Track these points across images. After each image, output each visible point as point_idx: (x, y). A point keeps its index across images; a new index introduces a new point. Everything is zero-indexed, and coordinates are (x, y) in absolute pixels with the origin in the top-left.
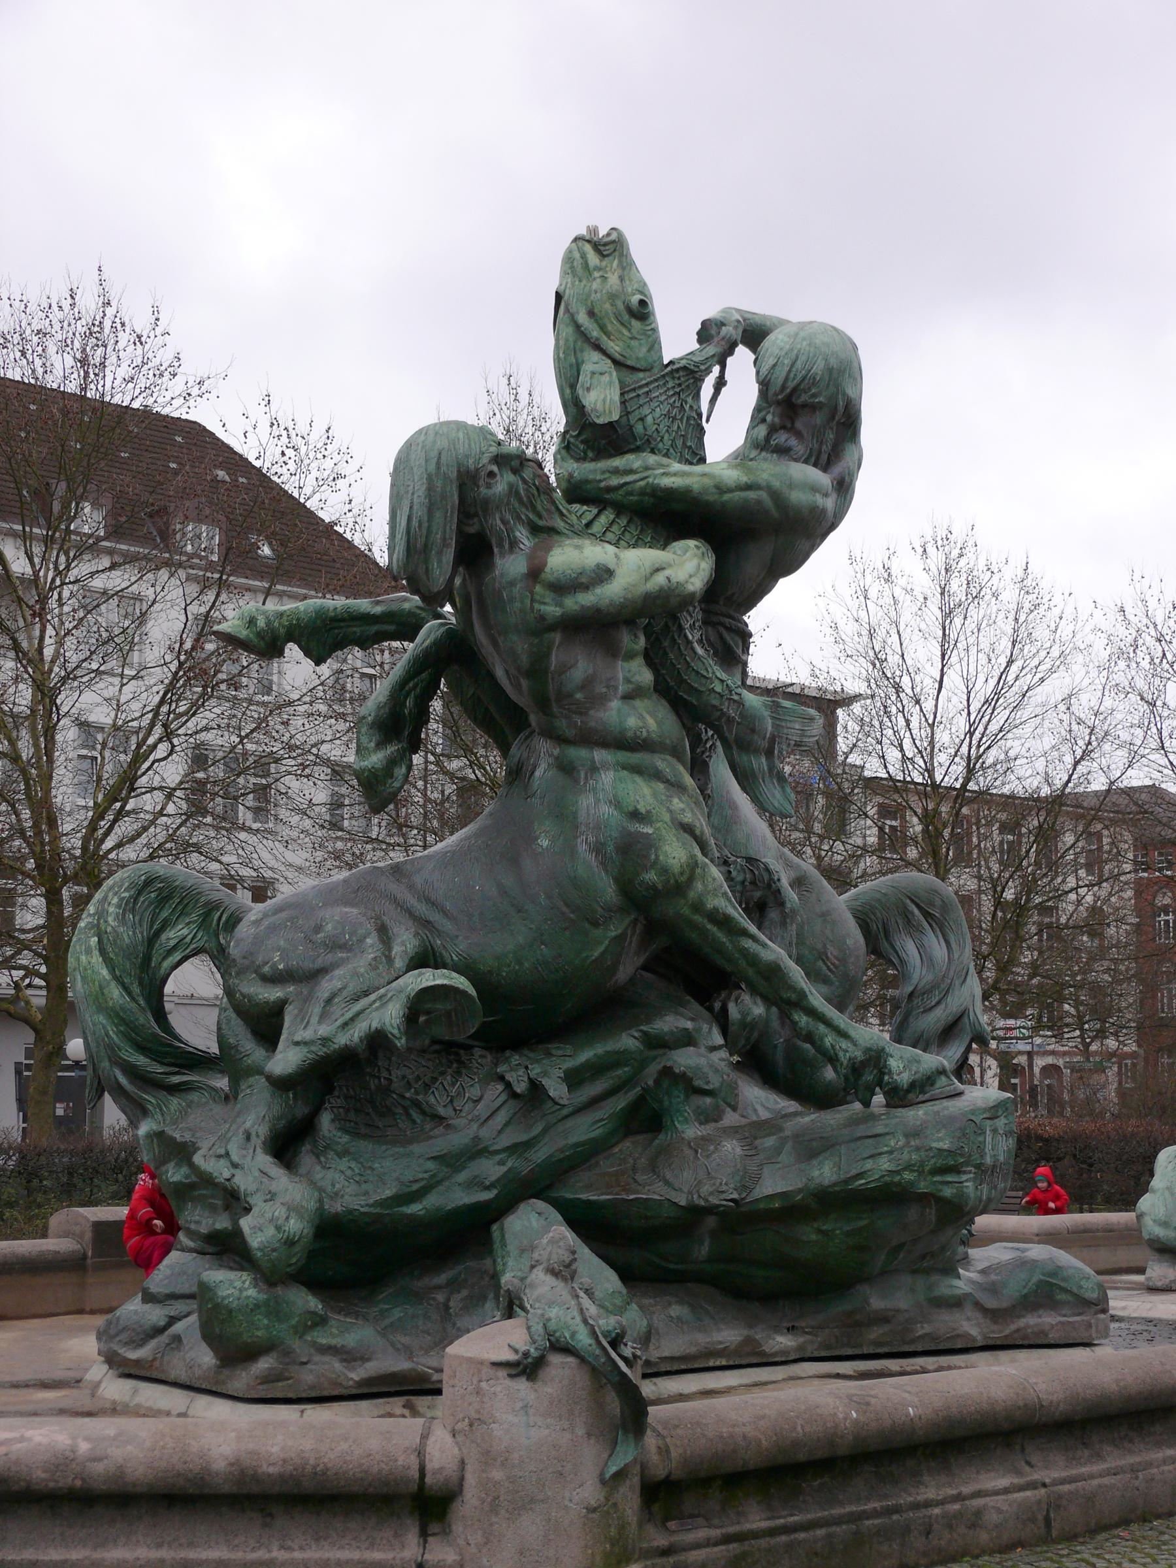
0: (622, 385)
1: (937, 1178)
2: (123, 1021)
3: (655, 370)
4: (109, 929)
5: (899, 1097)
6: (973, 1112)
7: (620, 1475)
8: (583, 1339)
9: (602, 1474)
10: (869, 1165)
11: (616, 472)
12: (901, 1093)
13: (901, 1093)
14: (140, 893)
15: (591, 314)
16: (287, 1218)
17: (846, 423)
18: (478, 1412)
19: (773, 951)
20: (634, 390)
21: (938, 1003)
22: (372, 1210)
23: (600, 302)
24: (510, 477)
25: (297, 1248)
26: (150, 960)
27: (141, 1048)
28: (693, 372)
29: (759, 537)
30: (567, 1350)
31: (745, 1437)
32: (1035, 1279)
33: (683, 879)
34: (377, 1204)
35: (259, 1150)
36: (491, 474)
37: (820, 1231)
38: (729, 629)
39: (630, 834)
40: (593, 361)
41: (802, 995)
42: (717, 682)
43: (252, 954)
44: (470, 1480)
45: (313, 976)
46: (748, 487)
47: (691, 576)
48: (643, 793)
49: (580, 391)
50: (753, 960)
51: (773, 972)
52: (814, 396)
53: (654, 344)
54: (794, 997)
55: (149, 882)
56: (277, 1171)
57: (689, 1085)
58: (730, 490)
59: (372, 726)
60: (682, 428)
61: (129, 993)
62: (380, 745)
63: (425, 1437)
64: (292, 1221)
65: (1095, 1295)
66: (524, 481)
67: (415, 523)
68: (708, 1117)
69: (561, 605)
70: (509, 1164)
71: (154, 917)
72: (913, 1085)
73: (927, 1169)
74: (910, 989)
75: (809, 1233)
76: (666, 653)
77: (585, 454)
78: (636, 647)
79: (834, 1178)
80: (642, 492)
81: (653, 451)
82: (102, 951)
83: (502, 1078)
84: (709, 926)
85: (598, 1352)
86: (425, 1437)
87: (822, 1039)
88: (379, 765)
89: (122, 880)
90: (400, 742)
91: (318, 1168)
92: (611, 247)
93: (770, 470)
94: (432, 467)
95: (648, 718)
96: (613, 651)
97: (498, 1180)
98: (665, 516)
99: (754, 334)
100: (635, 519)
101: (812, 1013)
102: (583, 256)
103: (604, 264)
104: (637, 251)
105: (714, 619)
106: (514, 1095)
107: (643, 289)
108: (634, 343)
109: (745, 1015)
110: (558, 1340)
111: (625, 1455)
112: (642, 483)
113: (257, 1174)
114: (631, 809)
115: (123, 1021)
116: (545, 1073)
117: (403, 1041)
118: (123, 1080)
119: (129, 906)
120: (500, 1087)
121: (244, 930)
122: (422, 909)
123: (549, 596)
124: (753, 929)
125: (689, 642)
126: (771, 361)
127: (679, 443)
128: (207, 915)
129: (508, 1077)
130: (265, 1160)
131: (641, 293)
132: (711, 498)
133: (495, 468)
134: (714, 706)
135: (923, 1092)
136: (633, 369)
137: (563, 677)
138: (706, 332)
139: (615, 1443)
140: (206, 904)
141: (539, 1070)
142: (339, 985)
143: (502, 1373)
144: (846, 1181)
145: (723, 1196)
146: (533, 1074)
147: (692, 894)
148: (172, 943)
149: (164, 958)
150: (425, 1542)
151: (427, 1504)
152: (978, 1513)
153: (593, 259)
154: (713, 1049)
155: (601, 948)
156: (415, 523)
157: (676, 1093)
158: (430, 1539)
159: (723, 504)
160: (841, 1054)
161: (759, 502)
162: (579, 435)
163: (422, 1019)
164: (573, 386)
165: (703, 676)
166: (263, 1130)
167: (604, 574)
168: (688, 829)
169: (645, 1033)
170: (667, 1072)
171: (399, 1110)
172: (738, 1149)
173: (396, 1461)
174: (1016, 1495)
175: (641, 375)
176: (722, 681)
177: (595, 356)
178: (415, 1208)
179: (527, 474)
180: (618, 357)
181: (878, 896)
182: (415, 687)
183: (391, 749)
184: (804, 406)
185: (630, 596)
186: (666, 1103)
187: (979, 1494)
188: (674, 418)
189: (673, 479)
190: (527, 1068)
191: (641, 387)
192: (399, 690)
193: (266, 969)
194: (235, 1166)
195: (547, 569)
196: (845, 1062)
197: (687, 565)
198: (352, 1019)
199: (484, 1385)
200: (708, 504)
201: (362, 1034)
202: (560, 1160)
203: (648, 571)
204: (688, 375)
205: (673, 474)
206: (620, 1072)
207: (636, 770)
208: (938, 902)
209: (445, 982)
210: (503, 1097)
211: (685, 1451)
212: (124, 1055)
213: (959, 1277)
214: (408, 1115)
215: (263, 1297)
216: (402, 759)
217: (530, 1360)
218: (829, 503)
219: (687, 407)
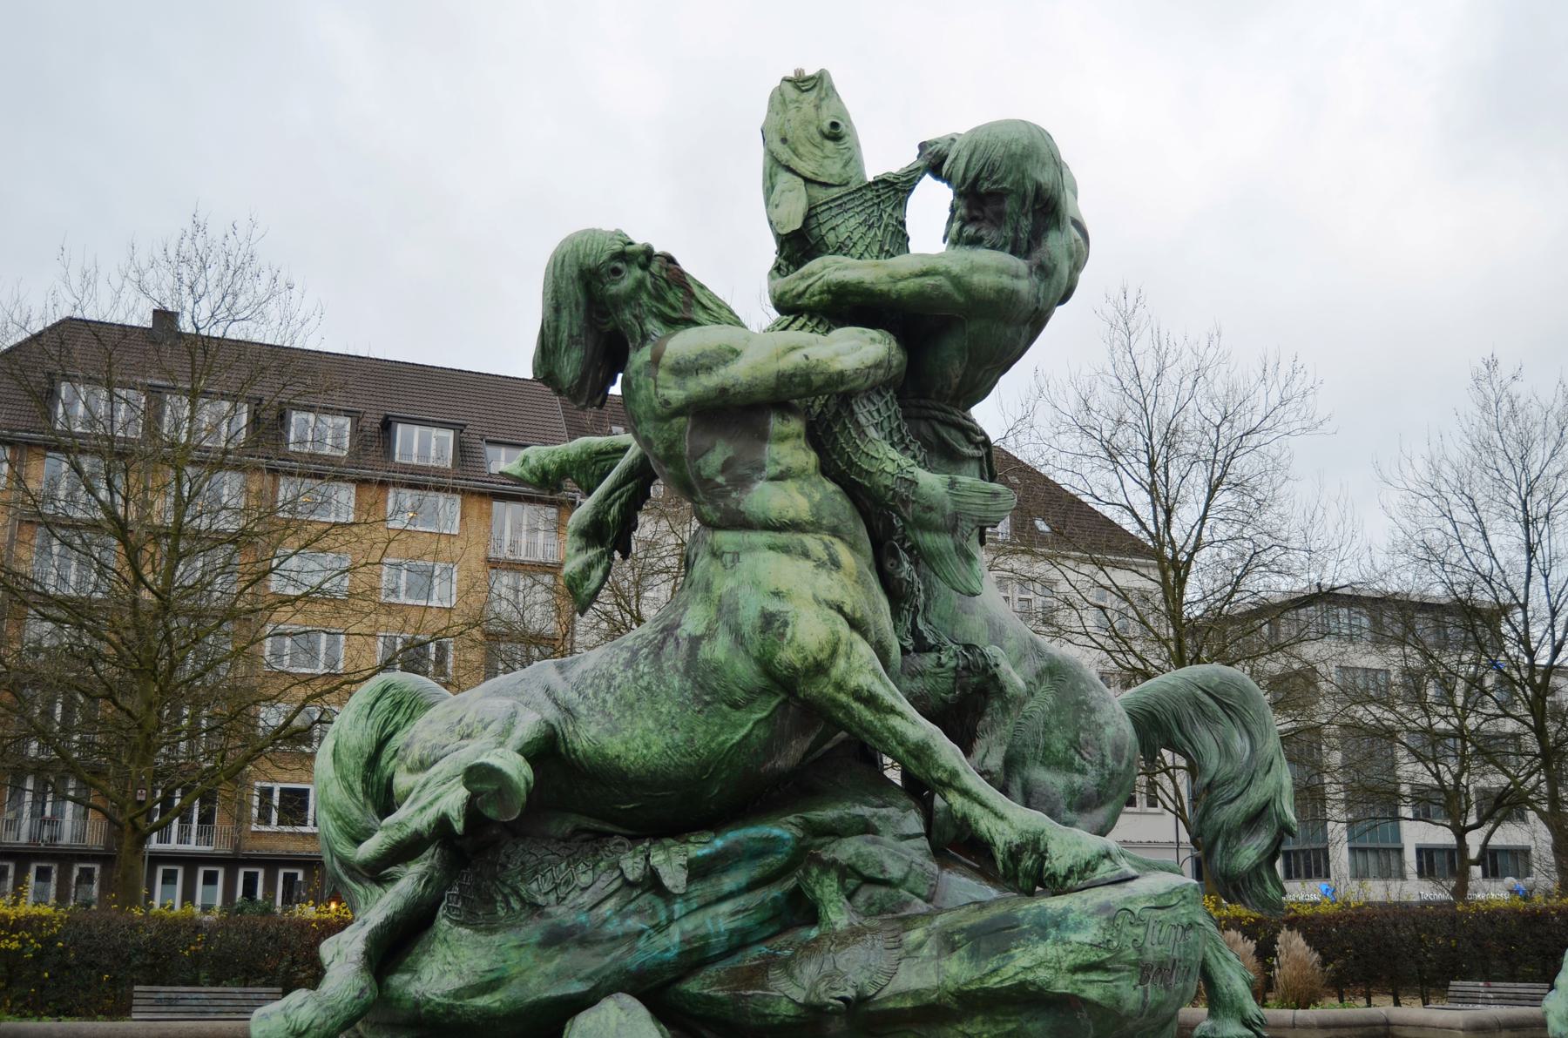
0: (809, 197)
1: (1080, 976)
2: (340, 816)
15: (784, 140)
21: (1241, 794)
22: (445, 1001)
24: (638, 273)
28: (893, 184)
33: (823, 656)
36: (616, 272)
40: (784, 178)
41: (954, 774)
42: (889, 462)
52: (995, 182)
53: (852, 159)
54: (945, 777)
55: (385, 691)
57: (855, 878)
58: (904, 278)
61: (350, 789)
66: (652, 275)
69: (682, 387)
73: (1065, 965)
74: (1206, 780)
76: (836, 439)
80: (821, 293)
92: (811, 83)
98: (845, 307)
101: (965, 793)
105: (925, 412)
108: (827, 162)
115: (340, 816)
123: (671, 380)
132: (884, 287)
133: (620, 265)
137: (701, 461)
145: (834, 994)
153: (791, 92)
155: (743, 732)
157: (827, 882)
159: (899, 294)
161: (937, 287)
169: (807, 821)
175: (836, 190)
177: (787, 176)
178: (482, 1001)
180: (809, 175)
182: (620, 497)
183: (592, 553)
184: (990, 194)
185: (758, 374)
186: (818, 892)
188: (871, 227)
195: (666, 354)
197: (856, 349)
200: (883, 295)
206: (770, 859)
207: (785, 549)
208: (1234, 692)
212: (339, 848)
214: (508, 903)
216: (599, 562)
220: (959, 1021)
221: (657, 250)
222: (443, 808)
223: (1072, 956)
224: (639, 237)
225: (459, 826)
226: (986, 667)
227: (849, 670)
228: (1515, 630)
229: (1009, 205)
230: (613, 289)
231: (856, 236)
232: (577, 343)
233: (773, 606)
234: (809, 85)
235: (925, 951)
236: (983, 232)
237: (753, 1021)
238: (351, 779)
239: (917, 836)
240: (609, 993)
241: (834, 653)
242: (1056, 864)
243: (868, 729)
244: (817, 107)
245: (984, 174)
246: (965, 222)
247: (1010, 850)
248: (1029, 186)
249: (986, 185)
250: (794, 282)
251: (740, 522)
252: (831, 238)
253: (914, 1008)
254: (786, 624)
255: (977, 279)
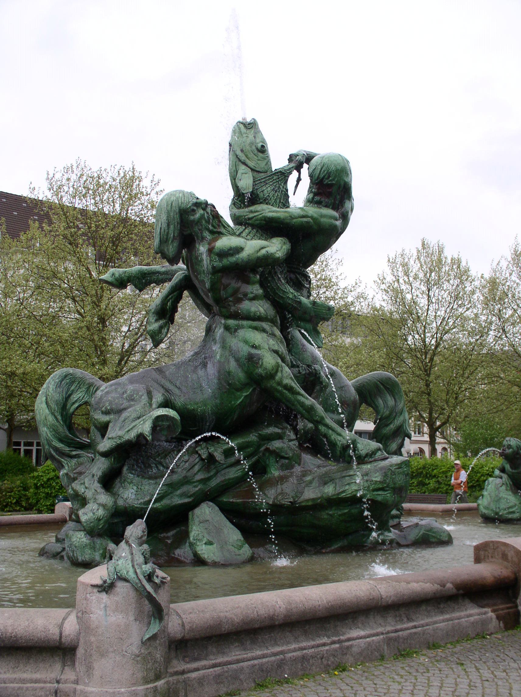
1: (375, 493)
3: (268, 172)
4: (50, 394)
5: (362, 460)
6: (391, 466)
7: (154, 637)
8: (131, 575)
9: (142, 639)
10: (347, 487)
11: (251, 212)
12: (362, 458)
13: (362, 458)
14: (62, 380)
15: (242, 151)
16: (98, 509)
17: (345, 191)
18: (85, 608)
19: (311, 400)
20: (259, 180)
23: (247, 148)
24: (202, 212)
25: (102, 522)
26: (66, 406)
27: (61, 441)
28: (284, 173)
29: (311, 239)
30: (126, 580)
31: (226, 617)
32: (421, 533)
34: (141, 504)
35: (96, 482)
37: (328, 514)
38: (299, 274)
39: (252, 354)
40: (242, 168)
41: (322, 418)
43: (99, 403)
44: (82, 641)
45: (119, 412)
46: (303, 217)
47: (277, 251)
48: (257, 337)
49: (237, 180)
50: (302, 405)
51: (310, 410)
52: (331, 181)
53: (268, 163)
55: (66, 376)
56: (100, 490)
57: (278, 455)
58: (296, 218)
59: (153, 313)
60: (279, 195)
61: (57, 419)
62: (156, 321)
63: (64, 619)
64: (100, 511)
65: (447, 539)
67: (163, 230)
68: (285, 467)
69: (221, 261)
70: (199, 487)
71: (68, 389)
72: (367, 455)
75: (324, 515)
77: (241, 206)
78: (255, 279)
79: (333, 493)
80: (261, 219)
81: (267, 204)
82: (47, 403)
83: (197, 452)
84: (284, 391)
85: (137, 581)
86: (64, 619)
87: (330, 436)
88: (156, 329)
89: (56, 375)
90: (165, 319)
91: (121, 488)
93: (313, 211)
94: (169, 208)
95: (261, 307)
96: (247, 281)
97: (194, 494)
98: (269, 228)
99: (309, 158)
100: (259, 230)
101: (327, 426)
102: (240, 129)
103: (248, 132)
104: (262, 127)
106: (202, 460)
107: (264, 141)
109: (305, 426)
110: (121, 575)
111: (155, 628)
112: (261, 216)
113: (93, 491)
114: (252, 344)
116: (216, 450)
117: (150, 437)
118: (54, 454)
119: (59, 385)
120: (197, 456)
121: (99, 393)
122: (168, 385)
124: (303, 392)
125: (279, 278)
126: (314, 168)
127: (278, 201)
128: (88, 388)
129: (199, 452)
130: (97, 486)
131: (263, 142)
132: (288, 221)
134: (289, 303)
135: (371, 457)
136: (259, 172)
138: (291, 158)
139: (149, 623)
140: (88, 384)
141: (213, 449)
142: (128, 415)
143: (95, 590)
144: (338, 494)
145: (286, 500)
146: (210, 451)
147: (277, 378)
148: (75, 399)
149: (72, 406)
150: (64, 669)
151: (61, 650)
152: (348, 648)
154: (291, 440)
156: (163, 230)
158: (66, 668)
160: (338, 442)
162: (238, 199)
163: (158, 428)
164: (235, 179)
165: (284, 291)
166: (100, 473)
167: (239, 250)
168: (276, 352)
170: (267, 449)
171: (154, 465)
172: (308, 482)
173: (49, 631)
174: (368, 639)
175: (263, 174)
176: (292, 293)
177: (243, 167)
179: (209, 210)
180: (252, 167)
181: (367, 381)
182: (171, 298)
183: (161, 322)
186: (267, 462)
187: (349, 640)
188: (276, 191)
189: (273, 214)
190: (208, 448)
191: (262, 179)
192: (165, 299)
193: (103, 409)
194: (86, 488)
196: (340, 445)
197: (277, 247)
198: (132, 429)
199: (88, 595)
201: (135, 434)
202: (223, 485)
203: (258, 248)
204: (283, 175)
205: (268, 211)
207: (256, 328)
209: (166, 413)
210: (197, 460)
211: (193, 625)
212: (54, 443)
213: (390, 532)
215: (88, 542)
216: (165, 326)
217: (106, 584)
218: (338, 223)
219: (281, 187)
220: (327, 509)
221: (209, 202)
222: (140, 431)
223: (373, 486)
224: (202, 196)
225: (149, 438)
226: (316, 374)
227: (281, 379)
228: (420, 336)
229: (334, 190)
230: (192, 218)
231: (271, 195)
232: (176, 239)
233: (254, 351)
234: (250, 126)
235: (314, 484)
236: (323, 199)
237: (252, 511)
238: (56, 414)
239: (294, 440)
240: (203, 501)
241: (277, 371)
242: (361, 452)
243: (288, 400)
244: (255, 137)
245: (326, 177)
246: (315, 194)
247: (343, 447)
248: (342, 183)
249: (326, 181)
250: (244, 212)
251: (236, 316)
252: (261, 195)
253: (312, 505)
254: (259, 359)
255: (323, 220)
